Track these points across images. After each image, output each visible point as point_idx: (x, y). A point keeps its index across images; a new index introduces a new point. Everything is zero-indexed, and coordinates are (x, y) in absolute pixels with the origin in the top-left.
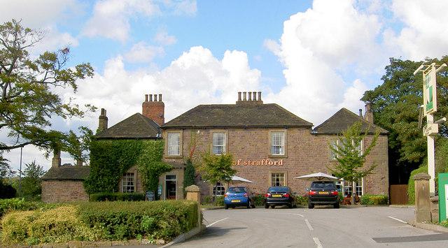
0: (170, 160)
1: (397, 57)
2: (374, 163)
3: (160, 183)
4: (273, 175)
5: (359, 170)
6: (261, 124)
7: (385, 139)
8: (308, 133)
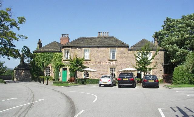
0: (65, 61)
1: (169, 17)
2: (156, 63)
3: (60, 71)
4: (111, 68)
5: (148, 67)
6: (106, 45)
7: (163, 52)
8: (127, 50)
